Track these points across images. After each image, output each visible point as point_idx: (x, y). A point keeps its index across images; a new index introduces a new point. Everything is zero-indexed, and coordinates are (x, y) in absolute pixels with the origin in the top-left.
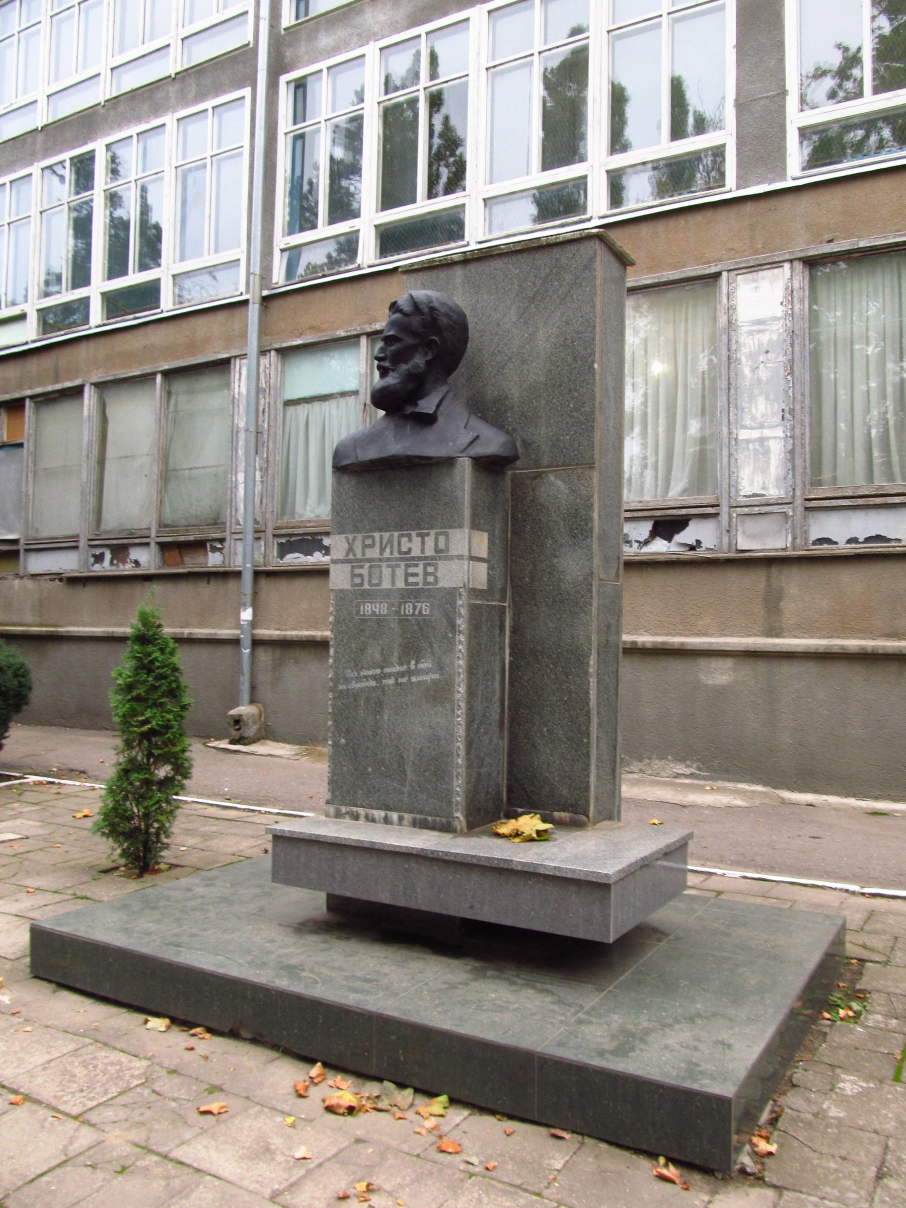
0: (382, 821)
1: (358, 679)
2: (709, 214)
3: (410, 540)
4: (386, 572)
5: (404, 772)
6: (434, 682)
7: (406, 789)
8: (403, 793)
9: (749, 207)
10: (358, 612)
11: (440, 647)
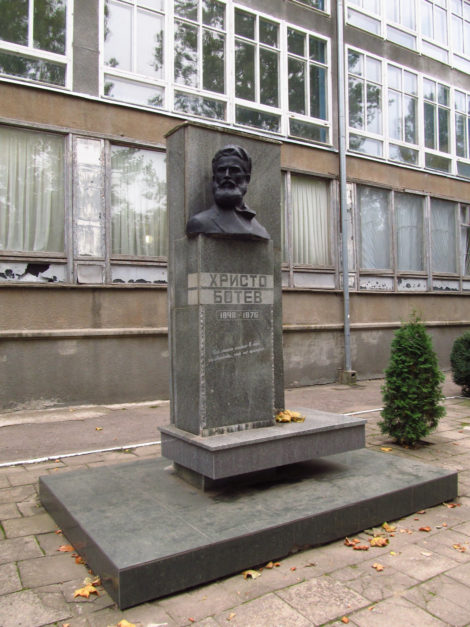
0: (237, 430)
1: (220, 355)
2: (62, 99)
3: (247, 279)
4: (235, 295)
5: (248, 401)
6: (261, 352)
7: (249, 410)
8: (248, 412)
9: (83, 104)
10: (219, 317)
11: (263, 334)
